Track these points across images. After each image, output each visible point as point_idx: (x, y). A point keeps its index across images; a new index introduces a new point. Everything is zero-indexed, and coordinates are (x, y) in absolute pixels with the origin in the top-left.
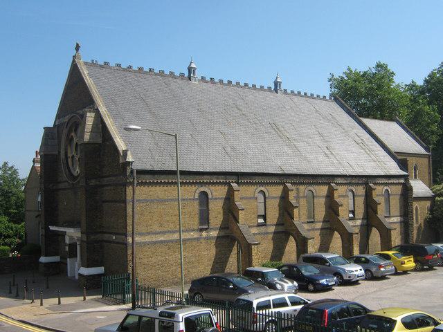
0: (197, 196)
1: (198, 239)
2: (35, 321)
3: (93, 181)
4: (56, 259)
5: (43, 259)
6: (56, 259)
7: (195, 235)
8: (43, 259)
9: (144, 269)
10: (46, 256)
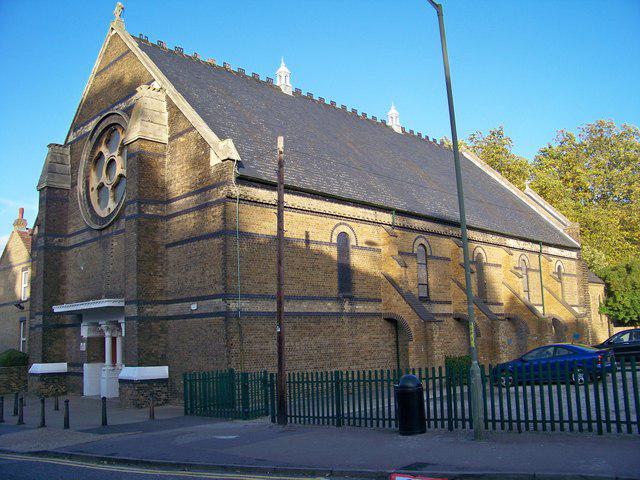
0: (335, 241)
1: (338, 315)
2: (129, 455)
3: (152, 207)
4: (62, 367)
5: (38, 368)
6: (62, 367)
7: (331, 307)
8: (38, 368)
9: (256, 362)
10: (45, 361)
